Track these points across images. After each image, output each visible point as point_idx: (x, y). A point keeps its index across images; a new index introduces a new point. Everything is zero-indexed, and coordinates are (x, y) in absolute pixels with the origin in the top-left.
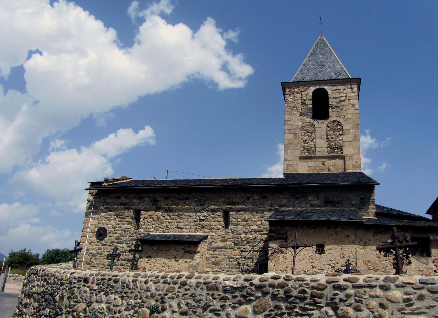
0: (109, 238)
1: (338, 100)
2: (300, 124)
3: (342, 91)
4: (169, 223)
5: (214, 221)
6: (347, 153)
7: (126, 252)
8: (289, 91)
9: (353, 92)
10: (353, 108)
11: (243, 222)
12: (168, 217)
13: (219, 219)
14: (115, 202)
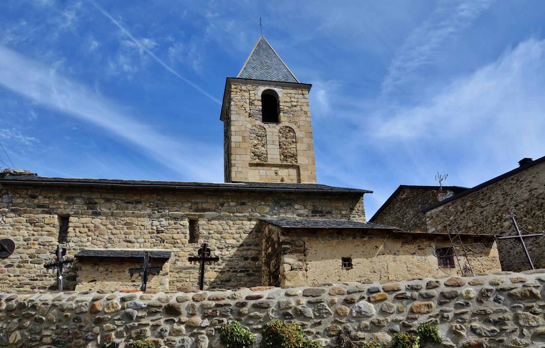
0: (19, 256)
1: (289, 105)
2: (249, 126)
3: (293, 95)
4: (112, 234)
5: (178, 233)
6: (301, 163)
7: (46, 276)
8: (236, 88)
9: (304, 98)
10: (306, 115)
11: (217, 235)
12: (112, 227)
13: (183, 230)
14: (28, 203)
